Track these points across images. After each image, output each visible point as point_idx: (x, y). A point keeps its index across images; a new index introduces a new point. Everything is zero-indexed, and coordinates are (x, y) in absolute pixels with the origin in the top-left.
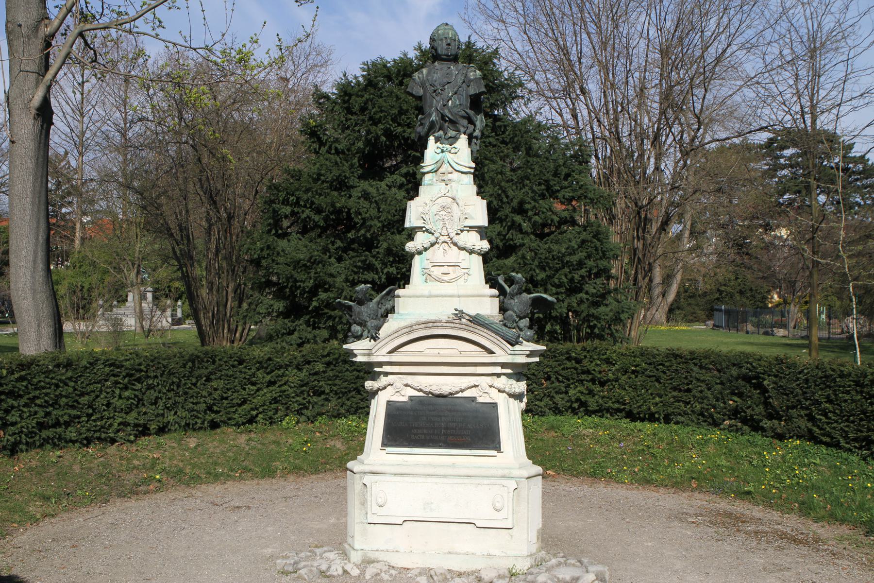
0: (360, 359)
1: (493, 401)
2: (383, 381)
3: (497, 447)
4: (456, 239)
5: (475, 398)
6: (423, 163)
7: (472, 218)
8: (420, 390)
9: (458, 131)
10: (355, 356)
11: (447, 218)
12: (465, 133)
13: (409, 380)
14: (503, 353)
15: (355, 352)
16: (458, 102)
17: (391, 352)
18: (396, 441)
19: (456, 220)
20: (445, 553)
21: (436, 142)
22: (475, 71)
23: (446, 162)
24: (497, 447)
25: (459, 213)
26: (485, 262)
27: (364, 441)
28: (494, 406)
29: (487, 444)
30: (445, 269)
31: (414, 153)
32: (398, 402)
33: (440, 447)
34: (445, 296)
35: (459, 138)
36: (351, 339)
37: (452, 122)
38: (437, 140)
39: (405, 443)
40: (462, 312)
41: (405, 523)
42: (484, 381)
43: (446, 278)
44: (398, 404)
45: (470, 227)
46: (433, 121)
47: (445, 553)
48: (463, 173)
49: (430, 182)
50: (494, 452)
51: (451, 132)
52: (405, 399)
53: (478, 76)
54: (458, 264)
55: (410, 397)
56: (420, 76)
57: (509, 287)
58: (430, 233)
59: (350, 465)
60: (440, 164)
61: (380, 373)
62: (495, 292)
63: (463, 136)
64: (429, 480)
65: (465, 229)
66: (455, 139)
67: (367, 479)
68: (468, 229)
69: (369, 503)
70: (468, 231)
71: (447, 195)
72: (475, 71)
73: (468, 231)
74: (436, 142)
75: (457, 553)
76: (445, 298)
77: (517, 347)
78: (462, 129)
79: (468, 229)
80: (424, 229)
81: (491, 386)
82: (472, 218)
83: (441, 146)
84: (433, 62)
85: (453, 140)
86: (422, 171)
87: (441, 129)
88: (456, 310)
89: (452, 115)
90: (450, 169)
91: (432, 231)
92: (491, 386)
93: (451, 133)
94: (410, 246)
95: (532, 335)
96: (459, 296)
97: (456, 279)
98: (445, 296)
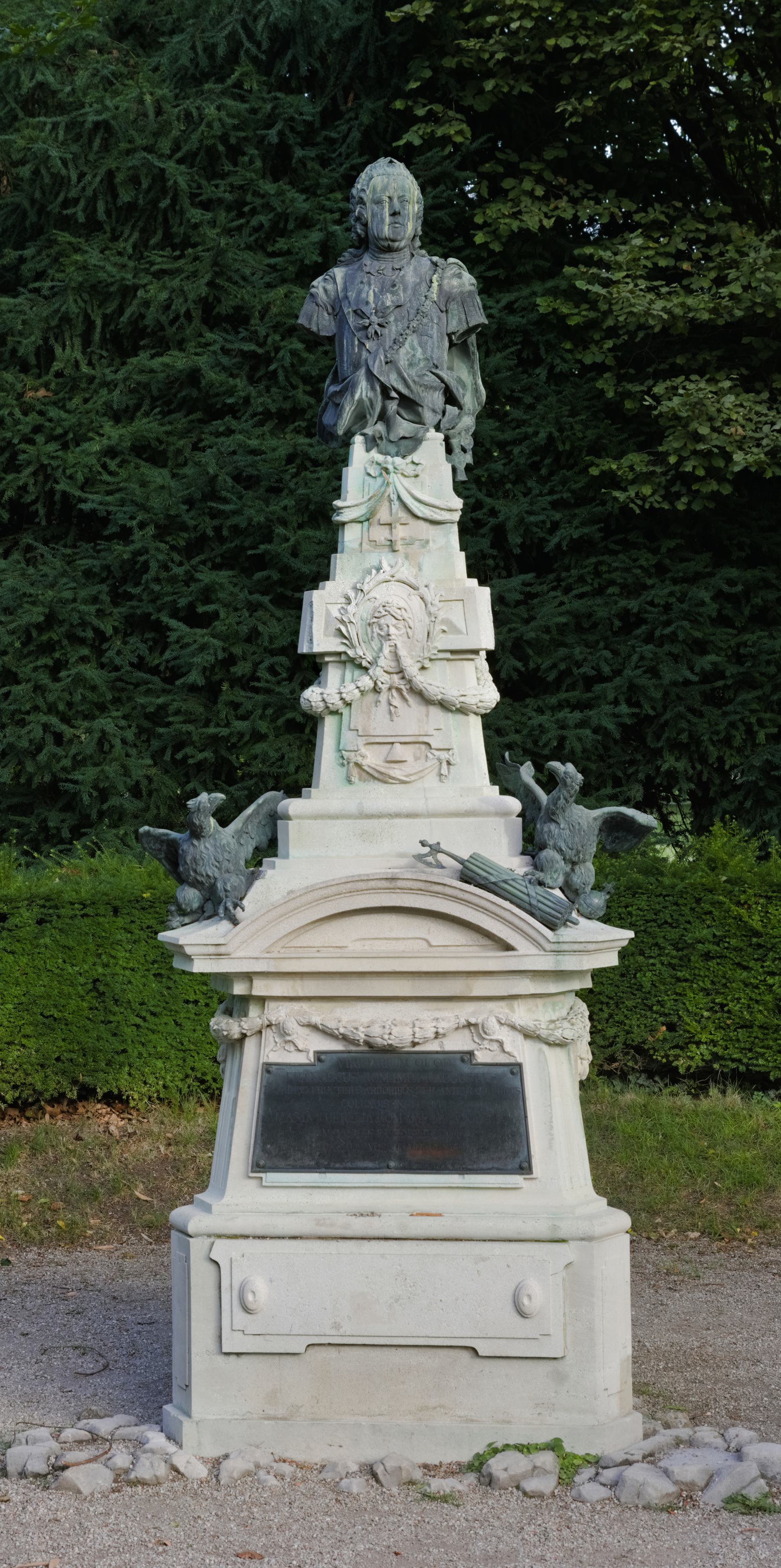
0: (199, 966)
1: (512, 1060)
2: (255, 1017)
3: (525, 1168)
4: (421, 680)
5: (471, 1054)
6: (339, 497)
8: (344, 1038)
9: (420, 421)
10: (189, 958)
12: (438, 428)
13: (318, 1014)
14: (534, 950)
15: (188, 950)
18: (285, 1157)
22: (459, 276)
24: (525, 1168)
26: (486, 727)
28: (516, 1069)
31: (601, 253)
34: (398, 815)
36: (176, 920)
37: (409, 404)
38: (372, 443)
39: (308, 1162)
40: (436, 849)
41: (311, 1351)
44: (288, 1070)
46: (360, 401)
51: (405, 424)
53: (468, 288)
56: (330, 287)
57: (548, 792)
58: (360, 666)
59: (178, 1214)
61: (245, 1000)
62: (514, 804)
63: (432, 433)
66: (414, 442)
67: (222, 1251)
72: (459, 276)
74: (368, 450)
76: (397, 821)
80: (343, 657)
81: (416, 476)
83: (380, 458)
84: (359, 257)
86: (338, 518)
88: (423, 843)
89: (408, 386)
90: (403, 515)
91: (364, 664)
92: (416, 476)
93: (404, 427)
94: (312, 696)
98: (398, 815)
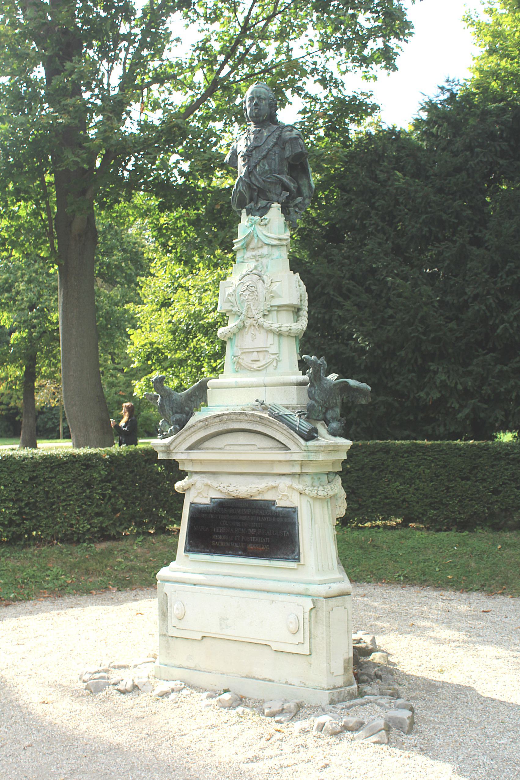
3: (297, 559)
5: (275, 501)
7: (279, 296)
11: (250, 298)
16: (267, 168)
17: (190, 448)
18: (197, 547)
19: (262, 299)
20: (243, 677)
21: (248, 215)
23: (255, 235)
24: (297, 559)
25: (265, 292)
27: (177, 542)
29: (286, 554)
30: (255, 356)
32: (200, 504)
33: (241, 556)
35: (270, 207)
42: (286, 482)
43: (255, 366)
45: (279, 306)
47: (243, 677)
48: (272, 246)
49: (242, 260)
50: (293, 565)
52: (207, 501)
54: (267, 349)
55: (211, 499)
60: (250, 237)
64: (226, 591)
65: (273, 309)
68: (276, 308)
69: (169, 618)
70: (278, 311)
71: (254, 272)
73: (278, 311)
75: (254, 678)
77: (310, 443)
78: (275, 197)
79: (276, 308)
82: (279, 296)
85: (265, 210)
87: (251, 200)
95: (338, 427)
96: (265, 386)
97: (265, 367)
